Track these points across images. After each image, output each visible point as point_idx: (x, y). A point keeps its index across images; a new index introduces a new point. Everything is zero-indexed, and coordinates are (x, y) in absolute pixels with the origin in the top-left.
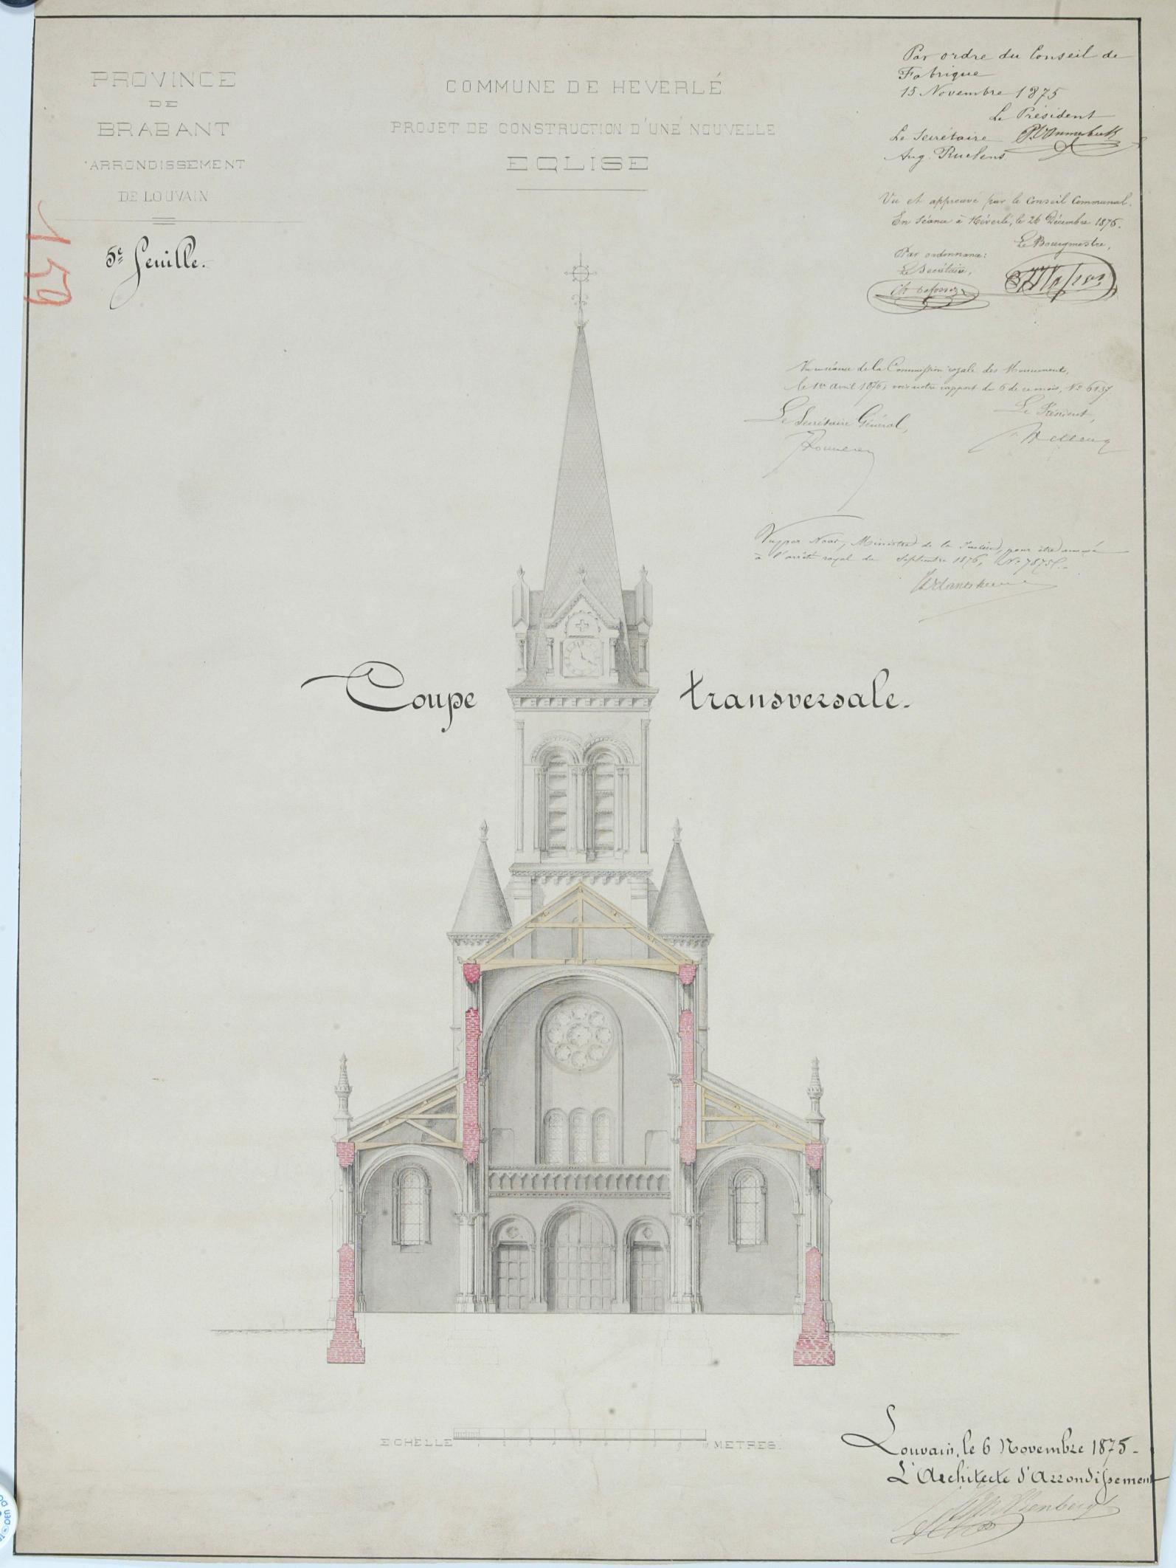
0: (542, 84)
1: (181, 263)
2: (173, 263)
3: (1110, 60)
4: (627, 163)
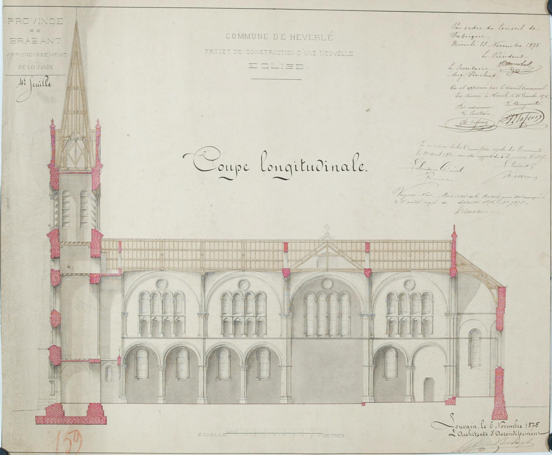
0: (308, 36)
1: (44, 84)
2: (42, 85)
3: (490, 30)
4: (295, 67)
